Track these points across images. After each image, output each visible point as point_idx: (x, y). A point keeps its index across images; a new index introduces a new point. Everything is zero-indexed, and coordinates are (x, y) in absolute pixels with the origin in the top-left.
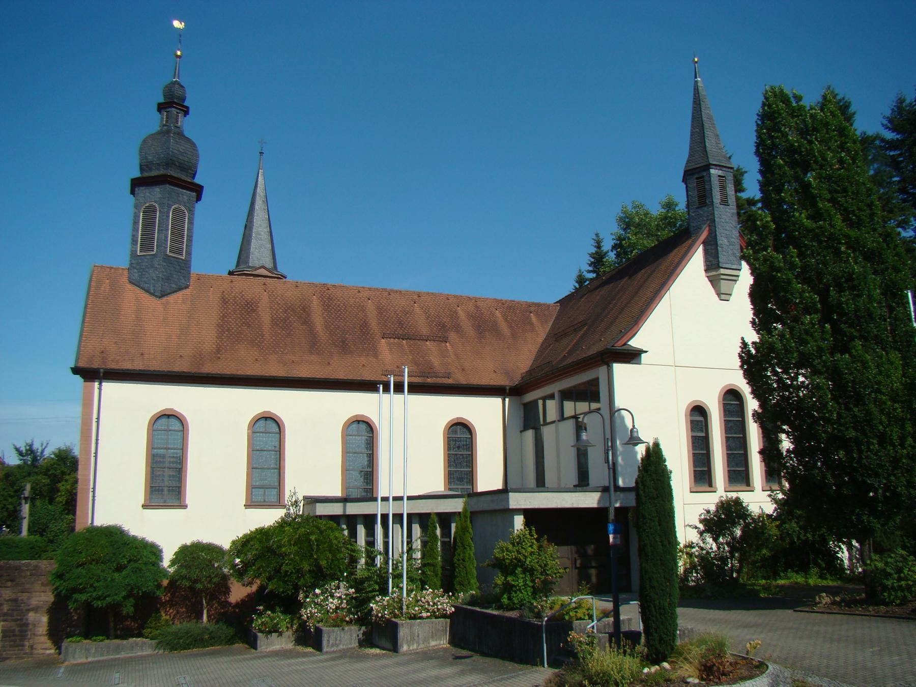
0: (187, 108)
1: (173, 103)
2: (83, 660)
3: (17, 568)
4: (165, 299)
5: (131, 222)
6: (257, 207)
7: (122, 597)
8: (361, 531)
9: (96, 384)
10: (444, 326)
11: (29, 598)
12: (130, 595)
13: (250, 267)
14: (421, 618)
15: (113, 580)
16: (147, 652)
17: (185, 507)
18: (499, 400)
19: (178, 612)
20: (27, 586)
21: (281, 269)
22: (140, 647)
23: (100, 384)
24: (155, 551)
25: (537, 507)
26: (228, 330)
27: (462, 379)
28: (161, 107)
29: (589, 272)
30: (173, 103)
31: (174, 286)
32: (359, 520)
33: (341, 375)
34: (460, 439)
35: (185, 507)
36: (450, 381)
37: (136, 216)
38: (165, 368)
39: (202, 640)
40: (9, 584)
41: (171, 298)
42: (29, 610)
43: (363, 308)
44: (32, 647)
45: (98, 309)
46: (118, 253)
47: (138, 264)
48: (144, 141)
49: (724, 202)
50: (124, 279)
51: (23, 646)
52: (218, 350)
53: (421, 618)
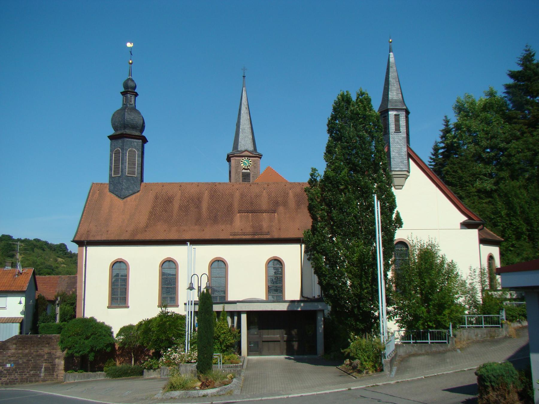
0: (136, 93)
1: (129, 90)
2: (73, 381)
3: (50, 338)
4: (125, 199)
5: (109, 159)
6: (242, 112)
7: (99, 353)
8: (236, 318)
9: (393, 173)
10: (278, 203)
11: (56, 352)
12: (92, 350)
13: (238, 151)
14: (191, 363)
15: (84, 343)
16: (103, 378)
17: (128, 307)
18: (299, 246)
19: (125, 359)
20: (55, 347)
21: (259, 151)
22: (100, 376)
23: (86, 248)
24: (108, 330)
25: (252, 310)
26: (155, 214)
27: (276, 235)
28: (123, 94)
29: (441, 142)
30: (129, 90)
31: (131, 192)
32: (235, 314)
33: (207, 237)
34: (276, 267)
35: (128, 307)
36: (268, 237)
37: (111, 156)
38: (117, 238)
39: (127, 373)
40: (47, 345)
41: (129, 199)
42: (56, 358)
43: (232, 196)
44: (57, 375)
45: (91, 208)
46: (103, 177)
47: (113, 181)
48: (114, 115)
49: (398, 130)
50: (107, 190)
51: (53, 375)
52: (147, 226)
53: (191, 363)
